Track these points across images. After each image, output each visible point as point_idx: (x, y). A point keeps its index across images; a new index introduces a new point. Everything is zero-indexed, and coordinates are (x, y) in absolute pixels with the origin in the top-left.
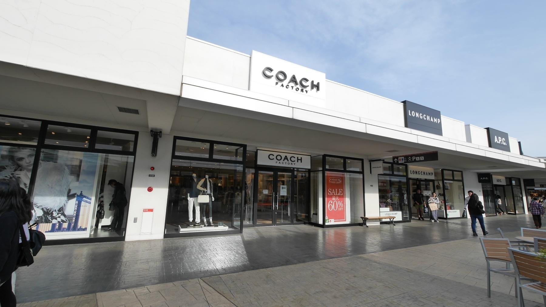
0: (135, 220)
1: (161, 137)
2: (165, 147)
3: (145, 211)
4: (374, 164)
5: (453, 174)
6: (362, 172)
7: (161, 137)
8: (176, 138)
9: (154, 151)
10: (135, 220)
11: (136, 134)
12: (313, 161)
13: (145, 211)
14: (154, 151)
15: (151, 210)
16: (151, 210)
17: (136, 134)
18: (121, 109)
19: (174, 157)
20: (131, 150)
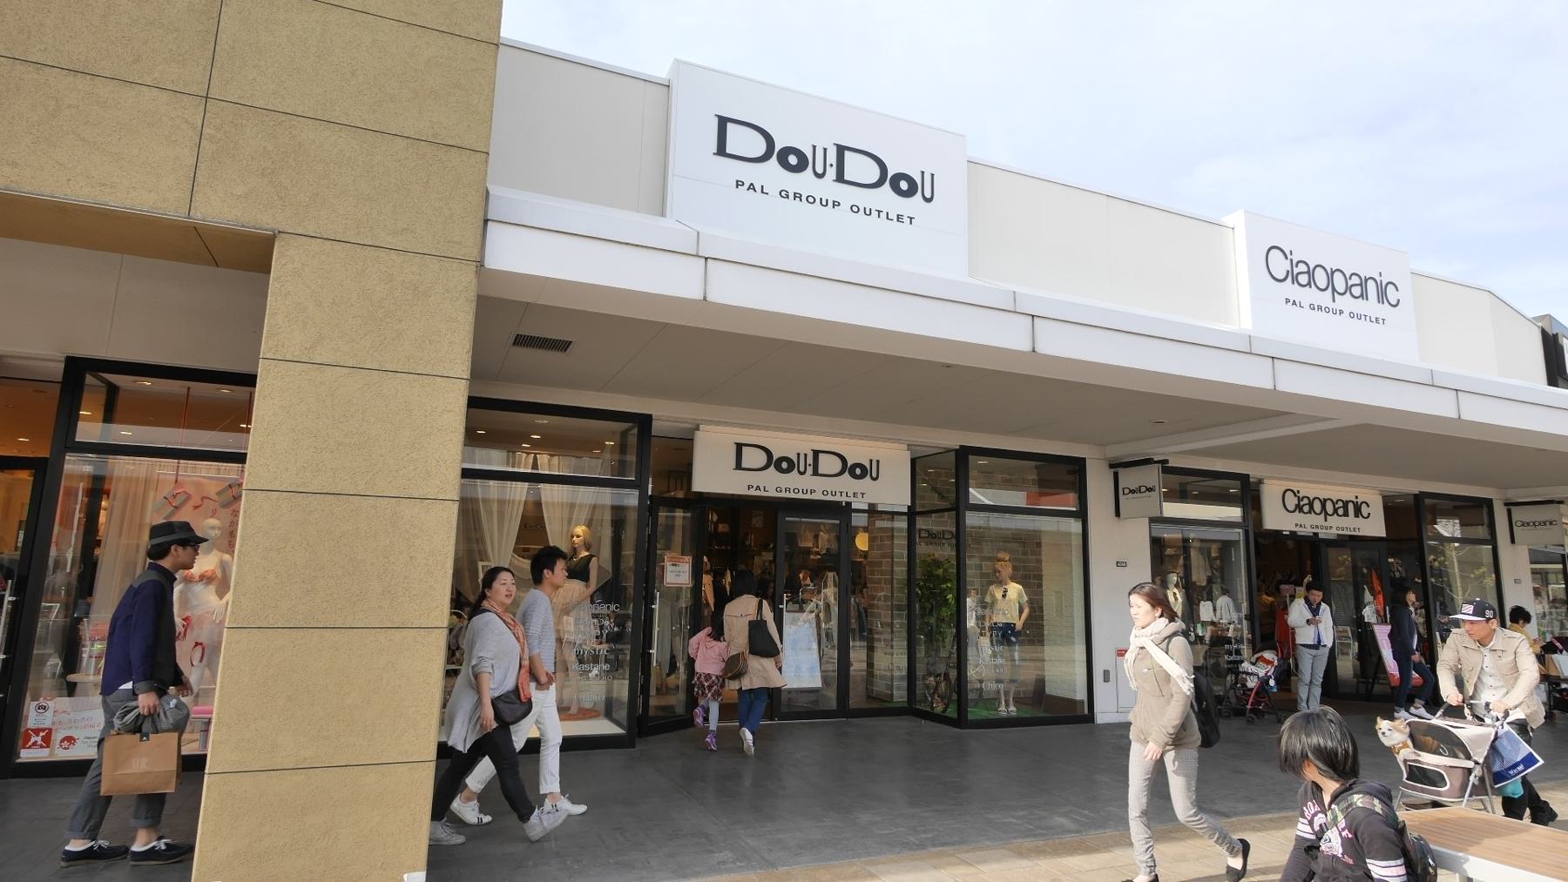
4: (1129, 478)
6: (1082, 514)
10: (1106, 678)
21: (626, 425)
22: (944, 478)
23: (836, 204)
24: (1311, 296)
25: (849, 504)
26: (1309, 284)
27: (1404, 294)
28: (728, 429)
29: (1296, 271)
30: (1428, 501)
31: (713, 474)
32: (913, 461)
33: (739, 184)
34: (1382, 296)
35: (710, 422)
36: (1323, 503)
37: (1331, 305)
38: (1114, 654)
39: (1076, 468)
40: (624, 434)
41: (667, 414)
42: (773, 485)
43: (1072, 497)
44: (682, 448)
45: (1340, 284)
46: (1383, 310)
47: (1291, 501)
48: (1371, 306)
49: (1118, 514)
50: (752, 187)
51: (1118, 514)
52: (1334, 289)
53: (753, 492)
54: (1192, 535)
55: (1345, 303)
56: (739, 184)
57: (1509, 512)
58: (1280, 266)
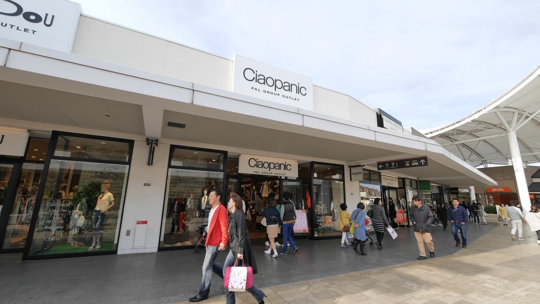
0: (128, 233)
1: (157, 145)
2: (162, 153)
3: (138, 223)
4: (354, 170)
5: (370, 174)
6: (343, 180)
7: (157, 145)
8: (173, 148)
9: (150, 162)
10: (128, 233)
11: (131, 143)
12: (33, 140)
13: (138, 223)
14: (150, 162)
15: (145, 222)
16: (145, 222)
17: (131, 143)
18: (183, 126)
19: (170, 166)
20: (127, 160)
21: (220, 154)
22: (305, 171)
23: (278, 95)
24: (265, 87)
25: (281, 177)
26: (264, 83)
27: (310, 91)
28: (18, 129)
29: (258, 78)
30: (316, 166)
31: (244, 168)
32: (30, 138)
33: (252, 88)
34: (299, 90)
35: (243, 154)
36: (269, 164)
37: (274, 92)
38: (135, 223)
39: (342, 167)
40: (219, 157)
41: (232, 151)
42: (261, 171)
43: (341, 176)
44: (235, 161)
45: (279, 84)
46: (299, 96)
47: (253, 163)
48: (293, 94)
49: (351, 180)
50: (256, 89)
51: (351, 180)
52: (276, 86)
53: (255, 173)
54: (84, 169)
55: (282, 92)
56: (252, 88)
57: (350, 170)
58: (250, 75)
